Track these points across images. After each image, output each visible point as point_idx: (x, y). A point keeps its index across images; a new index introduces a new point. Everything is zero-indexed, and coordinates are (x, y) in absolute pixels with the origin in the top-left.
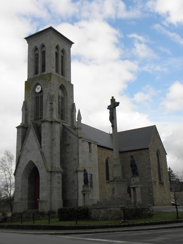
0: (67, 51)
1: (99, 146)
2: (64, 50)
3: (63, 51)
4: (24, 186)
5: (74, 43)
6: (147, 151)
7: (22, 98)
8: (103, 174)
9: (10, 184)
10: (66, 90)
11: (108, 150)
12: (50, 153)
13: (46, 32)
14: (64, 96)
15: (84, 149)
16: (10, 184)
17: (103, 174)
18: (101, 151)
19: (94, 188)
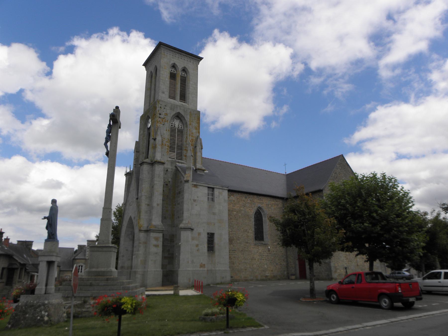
0: (190, 71)
1: (229, 191)
2: (186, 68)
3: (184, 70)
4: (127, 250)
5: (203, 58)
6: (320, 194)
7: (105, 136)
8: (248, 232)
9: (272, 242)
10: (185, 119)
11: (261, 197)
12: (148, 205)
13: (191, 58)
14: (184, 127)
15: (198, 197)
16: (272, 242)
17: (248, 232)
18: (244, 198)
19: (217, 253)
